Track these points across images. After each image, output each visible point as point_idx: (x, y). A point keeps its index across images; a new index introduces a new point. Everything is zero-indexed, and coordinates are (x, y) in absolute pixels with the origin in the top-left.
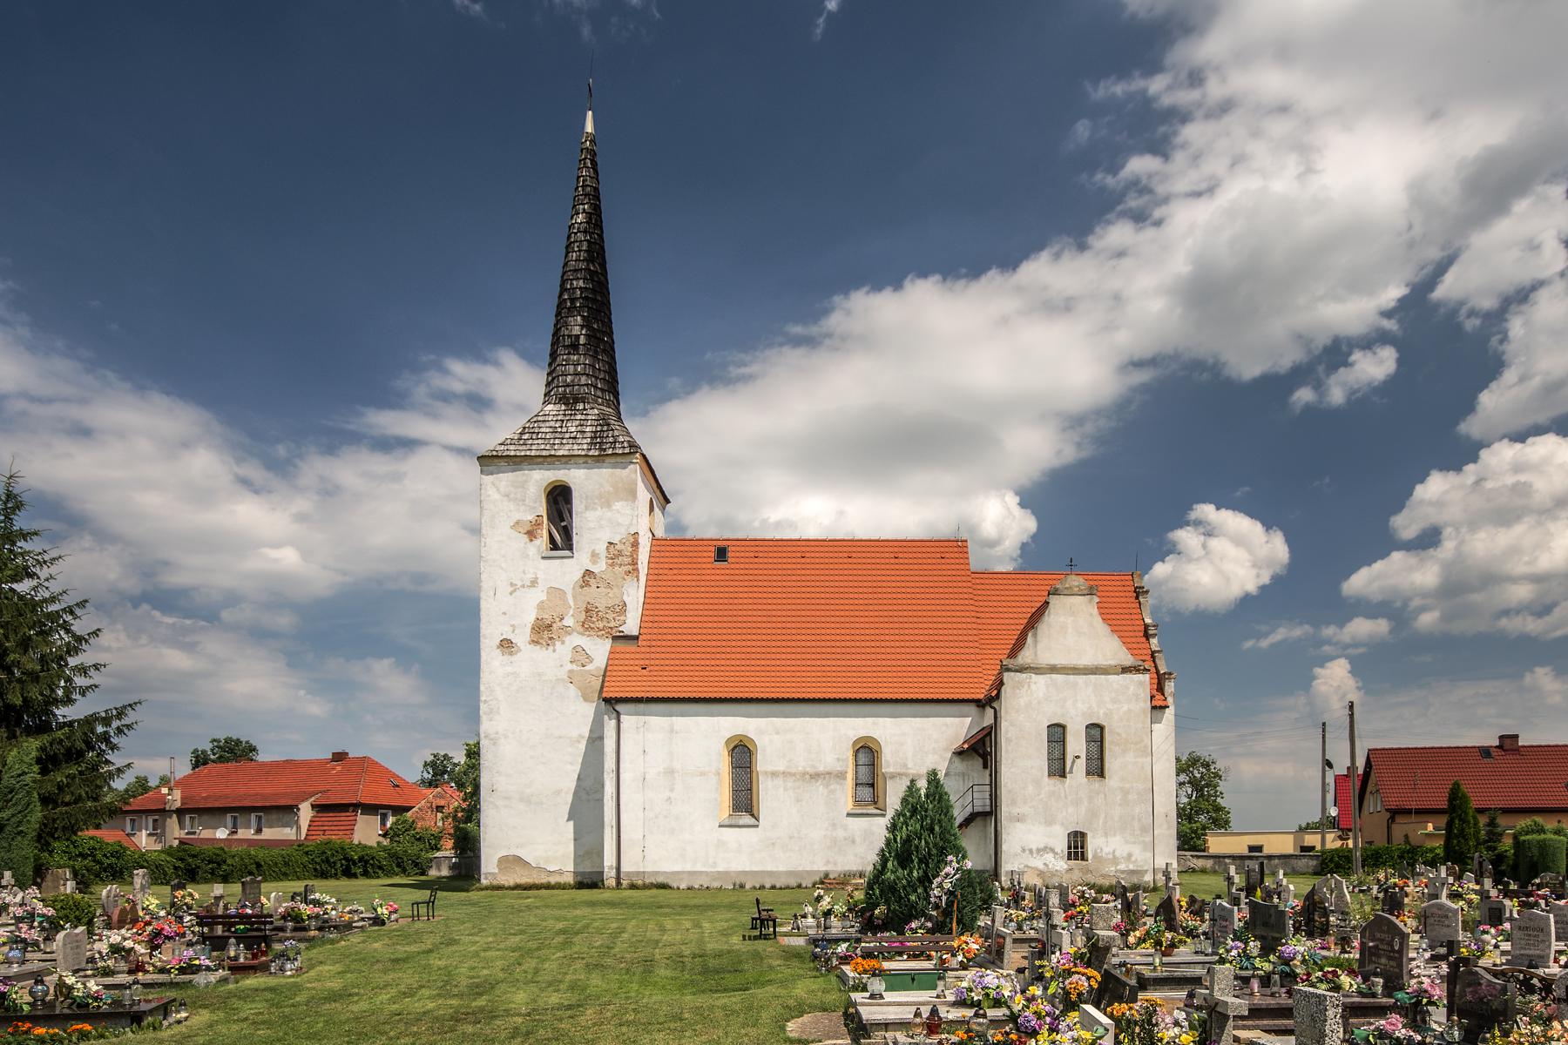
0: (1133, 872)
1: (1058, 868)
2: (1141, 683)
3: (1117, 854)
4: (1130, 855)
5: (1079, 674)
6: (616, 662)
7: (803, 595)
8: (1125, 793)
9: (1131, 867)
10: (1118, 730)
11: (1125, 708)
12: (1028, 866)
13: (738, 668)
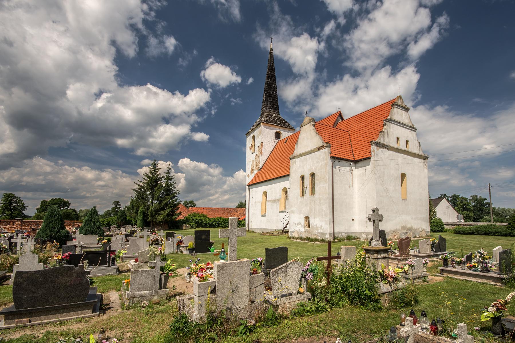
0: (322, 234)
1: (302, 231)
2: (325, 152)
3: (318, 226)
4: (321, 226)
5: (307, 155)
6: (368, 148)
7: (340, 139)
8: (320, 200)
9: (322, 231)
10: (318, 174)
11: (321, 164)
12: (295, 230)
13: (360, 148)
